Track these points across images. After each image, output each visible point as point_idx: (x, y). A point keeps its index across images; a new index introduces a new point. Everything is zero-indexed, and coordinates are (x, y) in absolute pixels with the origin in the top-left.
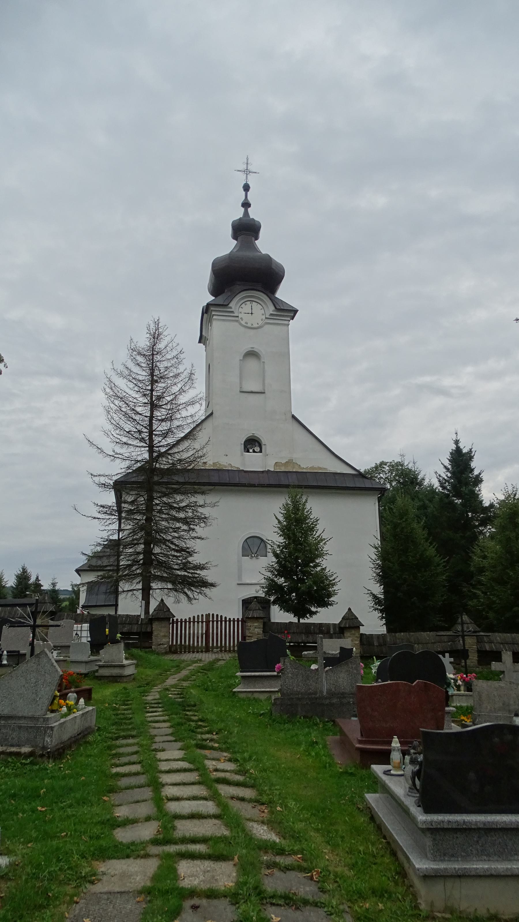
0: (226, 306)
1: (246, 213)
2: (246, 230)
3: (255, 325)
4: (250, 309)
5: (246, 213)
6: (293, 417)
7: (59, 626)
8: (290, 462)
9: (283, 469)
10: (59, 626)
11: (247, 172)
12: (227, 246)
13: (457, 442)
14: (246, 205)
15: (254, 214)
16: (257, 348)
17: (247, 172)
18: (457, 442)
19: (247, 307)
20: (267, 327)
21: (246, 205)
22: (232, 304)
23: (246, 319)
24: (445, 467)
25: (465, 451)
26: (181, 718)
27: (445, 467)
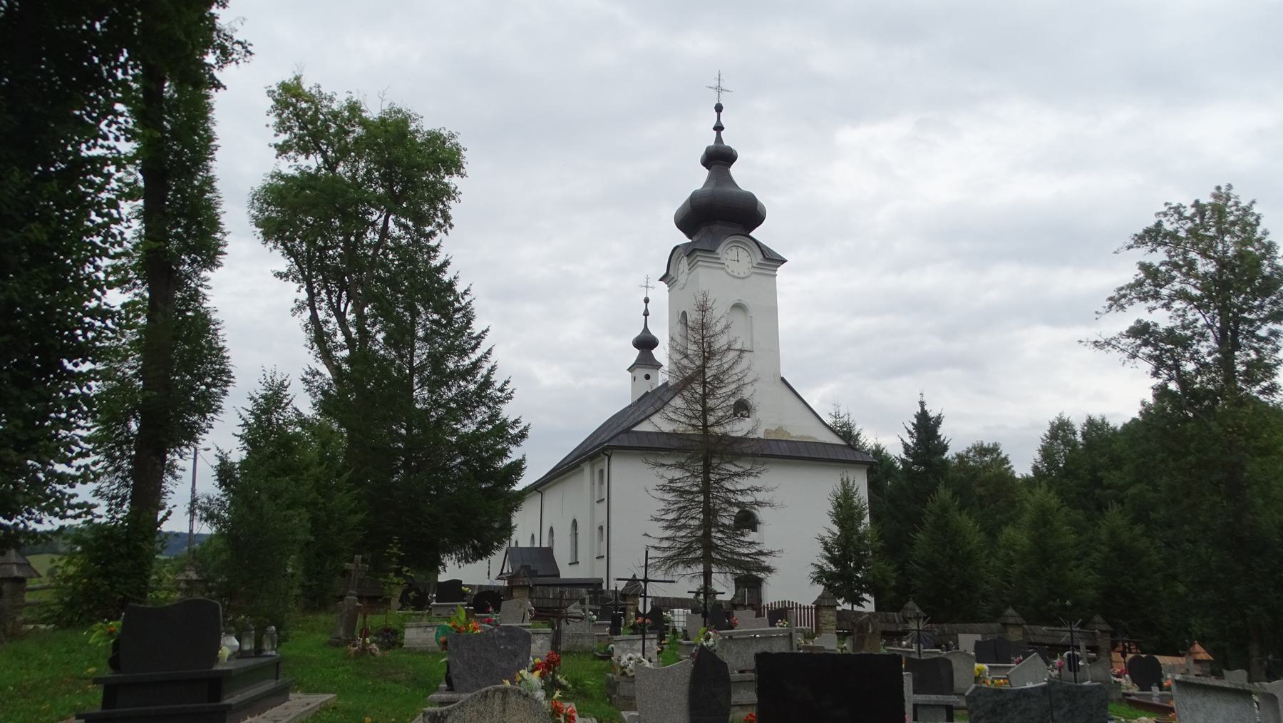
0: (712, 251)
1: (719, 139)
2: (719, 159)
3: (742, 275)
4: (734, 256)
5: (719, 139)
6: (783, 380)
7: (551, 530)
8: (779, 430)
9: (773, 437)
10: (551, 530)
11: (719, 89)
12: (698, 178)
13: (922, 404)
14: (719, 128)
15: (728, 140)
16: (745, 301)
17: (719, 89)
18: (922, 404)
19: (733, 254)
20: (753, 277)
21: (719, 128)
22: (719, 251)
23: (733, 267)
24: (769, 554)
25: (932, 414)
26: (349, 491)
27: (769, 554)
